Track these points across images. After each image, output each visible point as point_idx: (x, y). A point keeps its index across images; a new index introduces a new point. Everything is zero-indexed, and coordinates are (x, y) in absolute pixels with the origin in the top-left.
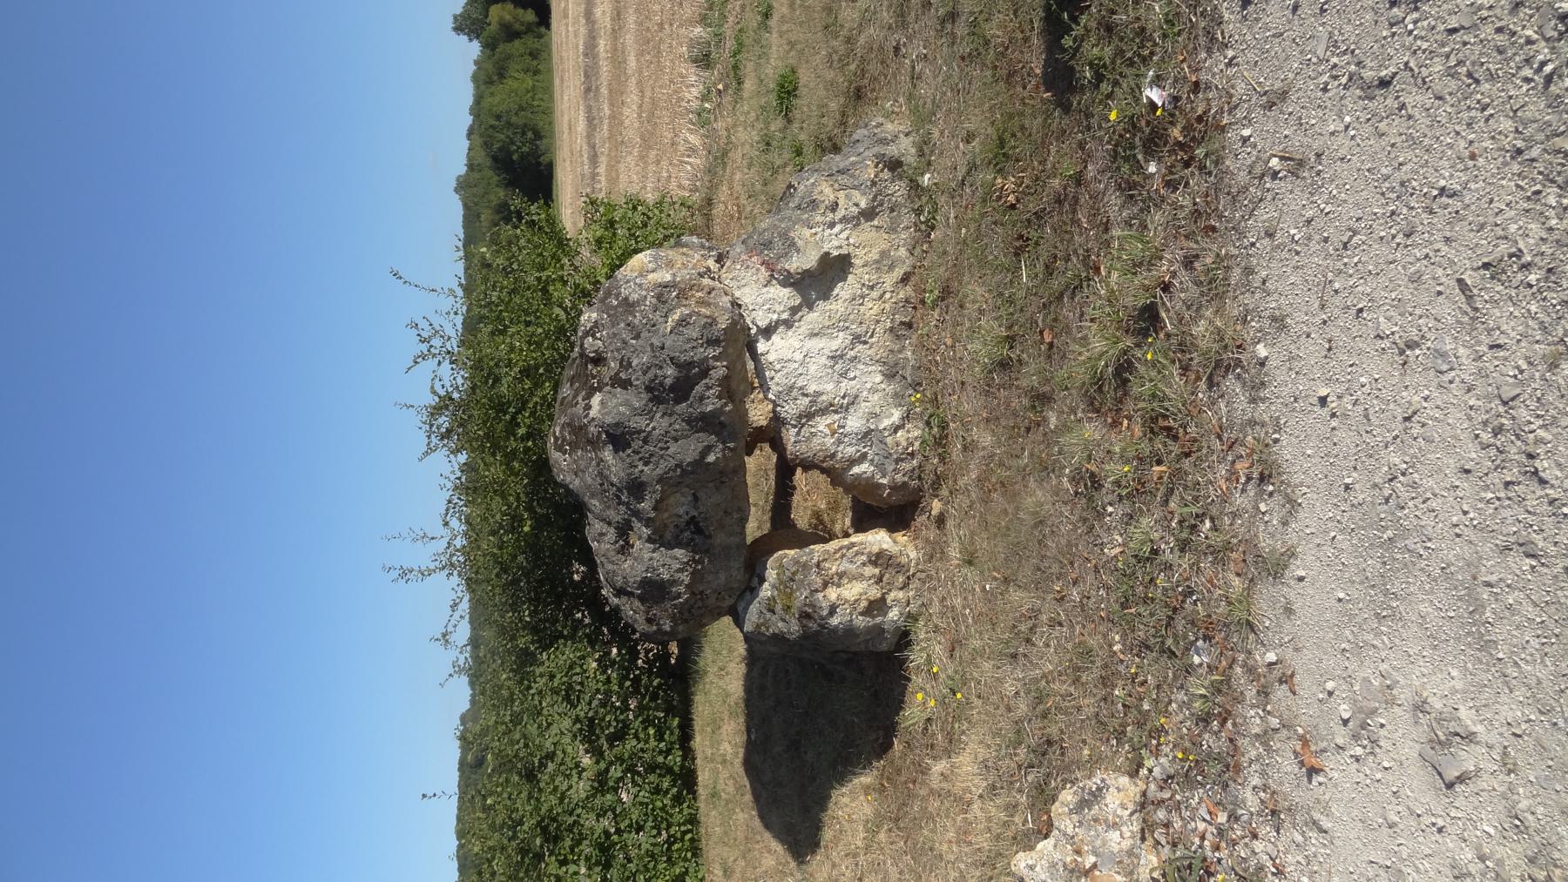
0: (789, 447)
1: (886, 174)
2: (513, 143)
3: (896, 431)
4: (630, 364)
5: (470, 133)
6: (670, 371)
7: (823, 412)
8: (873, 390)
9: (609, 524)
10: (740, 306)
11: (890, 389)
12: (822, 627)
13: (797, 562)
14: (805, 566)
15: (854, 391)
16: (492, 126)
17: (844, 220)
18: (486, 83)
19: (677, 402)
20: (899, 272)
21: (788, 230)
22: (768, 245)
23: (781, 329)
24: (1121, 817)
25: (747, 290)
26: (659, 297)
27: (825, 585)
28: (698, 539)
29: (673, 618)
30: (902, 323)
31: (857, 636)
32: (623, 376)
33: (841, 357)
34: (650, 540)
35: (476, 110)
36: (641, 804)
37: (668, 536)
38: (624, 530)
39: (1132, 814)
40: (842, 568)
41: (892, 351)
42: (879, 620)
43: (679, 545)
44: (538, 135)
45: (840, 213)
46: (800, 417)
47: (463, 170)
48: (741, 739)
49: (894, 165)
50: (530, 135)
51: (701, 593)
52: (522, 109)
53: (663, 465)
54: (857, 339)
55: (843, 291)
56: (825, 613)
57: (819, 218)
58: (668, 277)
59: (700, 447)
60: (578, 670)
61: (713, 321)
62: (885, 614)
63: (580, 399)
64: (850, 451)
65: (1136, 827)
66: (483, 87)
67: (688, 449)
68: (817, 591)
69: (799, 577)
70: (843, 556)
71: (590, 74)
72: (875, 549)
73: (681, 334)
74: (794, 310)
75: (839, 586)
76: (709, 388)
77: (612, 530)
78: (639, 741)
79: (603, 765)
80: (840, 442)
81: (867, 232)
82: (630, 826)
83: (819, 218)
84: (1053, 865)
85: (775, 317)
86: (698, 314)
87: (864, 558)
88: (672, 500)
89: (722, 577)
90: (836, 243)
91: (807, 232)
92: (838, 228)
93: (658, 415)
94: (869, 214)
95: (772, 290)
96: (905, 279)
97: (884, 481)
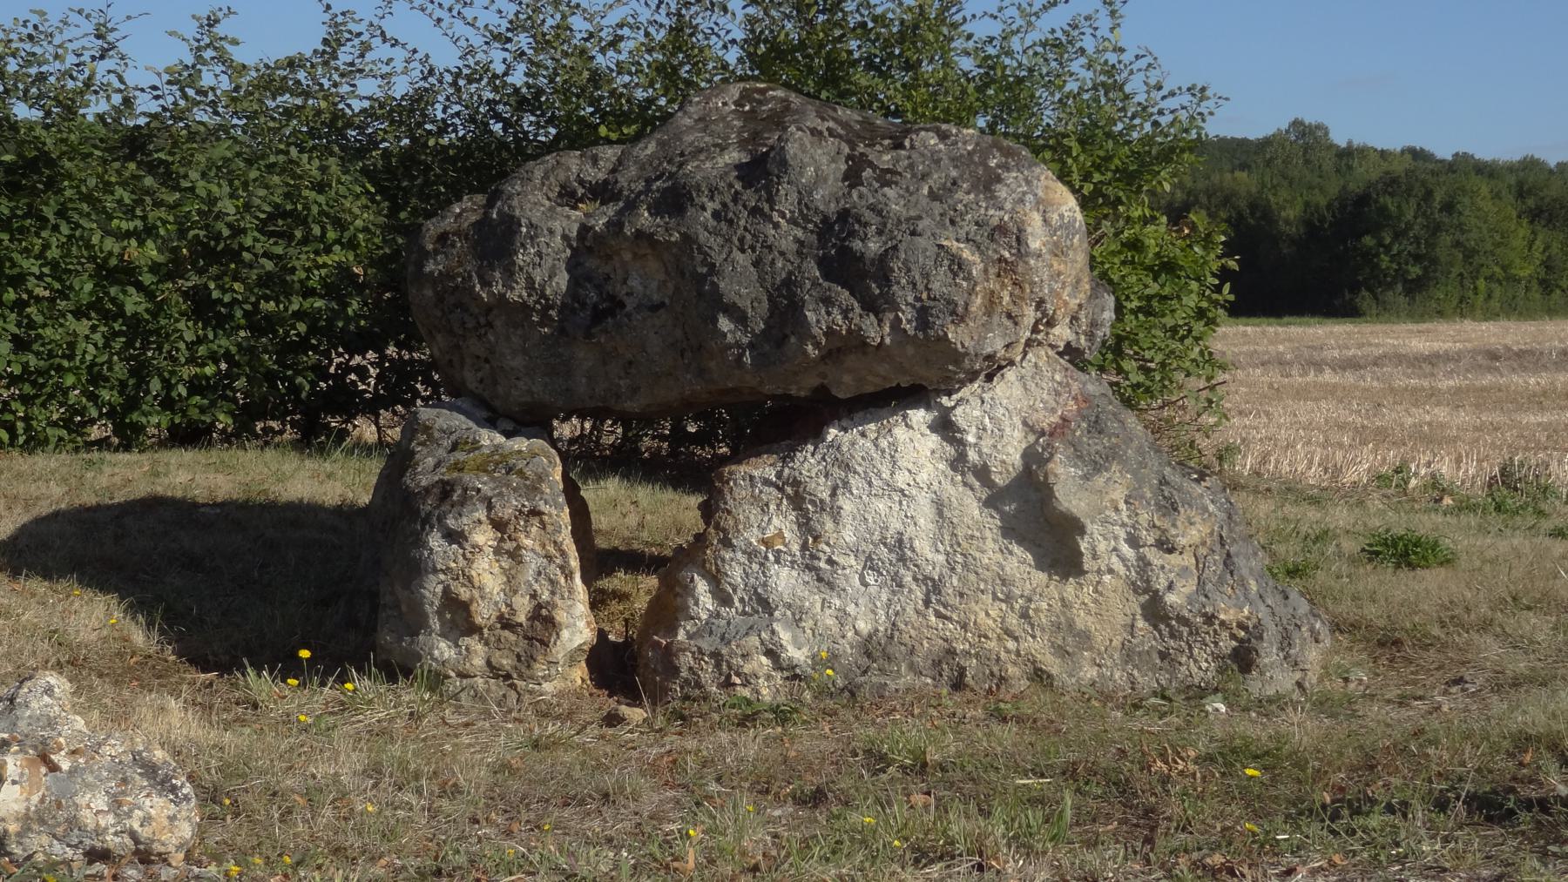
0: (743, 469)
1: (1227, 645)
2: (1397, 236)
3: (770, 653)
4: (888, 184)
5: (1417, 154)
6: (874, 246)
7: (805, 526)
8: (842, 617)
9: (613, 171)
10: (989, 378)
11: (846, 647)
12: (426, 521)
13: (541, 478)
14: (533, 489)
15: (841, 582)
16: (1429, 194)
17: (1144, 564)
18: (1520, 184)
19: (822, 263)
20: (1052, 664)
21: (1124, 462)
22: (1097, 427)
23: (950, 450)
24: (129, 815)
25: (1017, 391)
26: (1001, 229)
27: (499, 525)
28: (584, 316)
29: (448, 275)
30: (962, 671)
31: (407, 585)
32: (867, 173)
33: (902, 559)
34: (584, 229)
35: (1463, 166)
36: (72, 346)
37: (591, 263)
38: (602, 192)
39: (133, 835)
40: (527, 556)
41: (912, 651)
42: (435, 623)
43: (574, 282)
44: (1414, 287)
45: (1153, 556)
46: (796, 483)
47: (1339, 138)
48: (199, 494)
49: (1244, 658)
50: (1415, 271)
51: (490, 325)
52: (1469, 255)
53: (714, 242)
54: (934, 587)
55: (1018, 563)
56: (451, 522)
57: (1144, 517)
58: (1035, 244)
59: (745, 304)
60: (331, 235)
61: (960, 318)
62: (443, 635)
63: (831, 124)
64: (736, 574)
65: (111, 841)
66: (1512, 180)
67: (740, 283)
68: (490, 507)
69: (515, 480)
70: (549, 558)
71: (1525, 359)
72: (561, 616)
73: (937, 263)
74: (982, 473)
75: (497, 551)
76: (845, 313)
77: (601, 176)
78: (191, 346)
79: (147, 279)
80: (751, 554)
81: (1124, 608)
82: (32, 325)
83: (1144, 517)
84: (51, 723)
85: (971, 439)
86: (971, 292)
87: (546, 596)
88: (653, 265)
89: (518, 362)
90: (1102, 547)
91: (1119, 494)
92: (1126, 549)
93: (800, 233)
94: (1155, 611)
95: (1018, 434)
96: (1039, 676)
97: (681, 636)
